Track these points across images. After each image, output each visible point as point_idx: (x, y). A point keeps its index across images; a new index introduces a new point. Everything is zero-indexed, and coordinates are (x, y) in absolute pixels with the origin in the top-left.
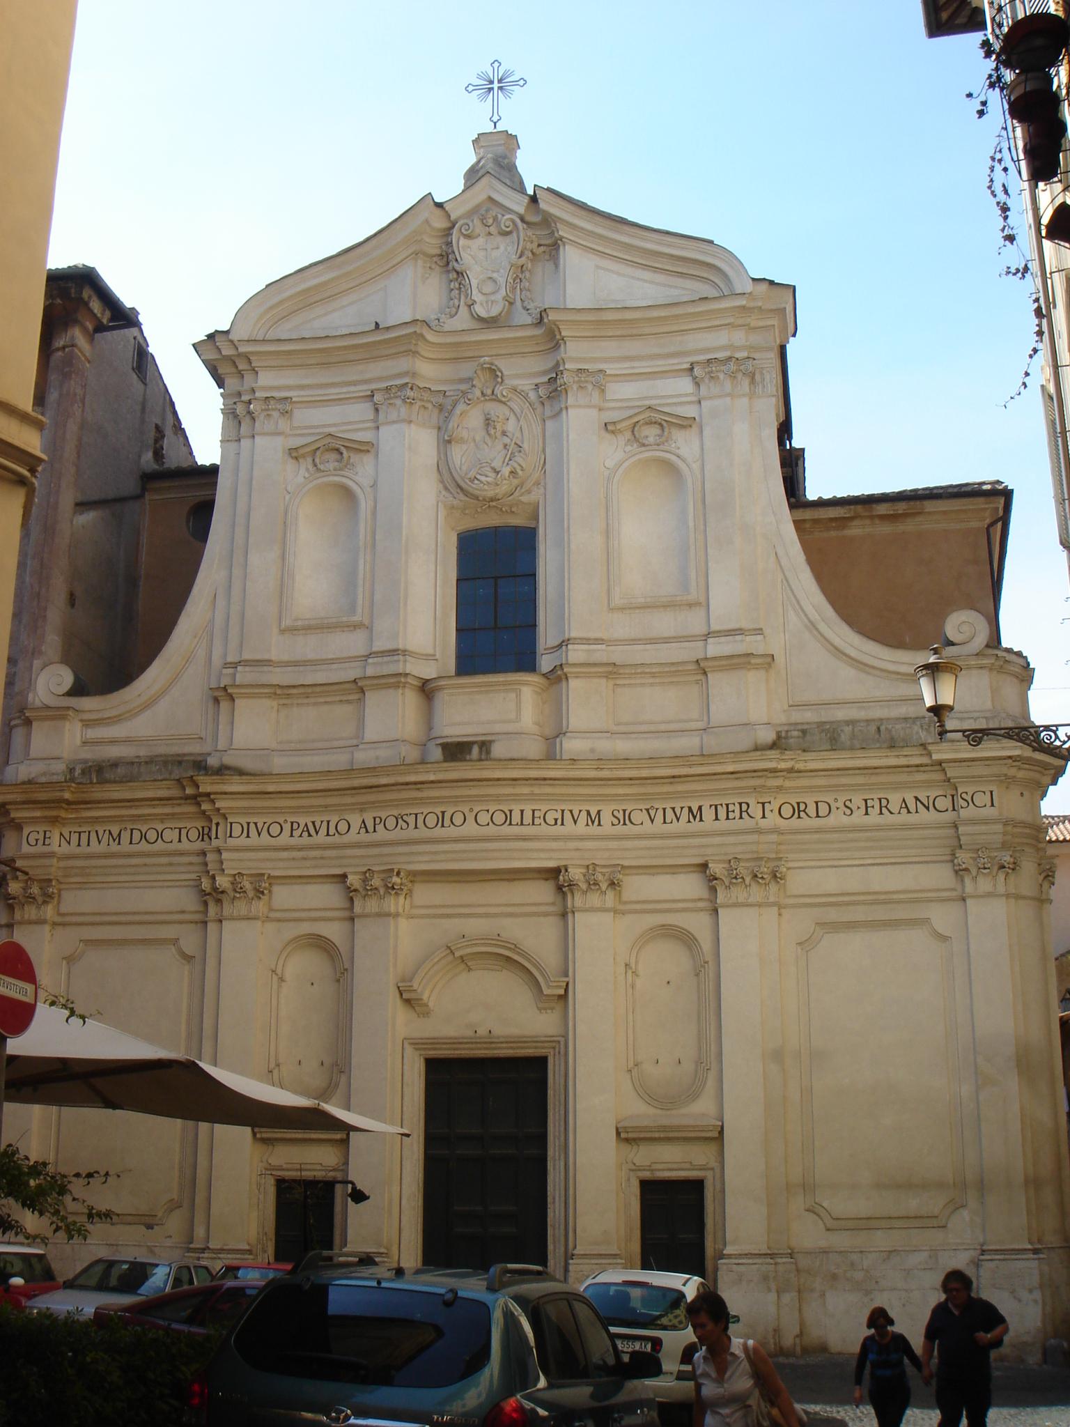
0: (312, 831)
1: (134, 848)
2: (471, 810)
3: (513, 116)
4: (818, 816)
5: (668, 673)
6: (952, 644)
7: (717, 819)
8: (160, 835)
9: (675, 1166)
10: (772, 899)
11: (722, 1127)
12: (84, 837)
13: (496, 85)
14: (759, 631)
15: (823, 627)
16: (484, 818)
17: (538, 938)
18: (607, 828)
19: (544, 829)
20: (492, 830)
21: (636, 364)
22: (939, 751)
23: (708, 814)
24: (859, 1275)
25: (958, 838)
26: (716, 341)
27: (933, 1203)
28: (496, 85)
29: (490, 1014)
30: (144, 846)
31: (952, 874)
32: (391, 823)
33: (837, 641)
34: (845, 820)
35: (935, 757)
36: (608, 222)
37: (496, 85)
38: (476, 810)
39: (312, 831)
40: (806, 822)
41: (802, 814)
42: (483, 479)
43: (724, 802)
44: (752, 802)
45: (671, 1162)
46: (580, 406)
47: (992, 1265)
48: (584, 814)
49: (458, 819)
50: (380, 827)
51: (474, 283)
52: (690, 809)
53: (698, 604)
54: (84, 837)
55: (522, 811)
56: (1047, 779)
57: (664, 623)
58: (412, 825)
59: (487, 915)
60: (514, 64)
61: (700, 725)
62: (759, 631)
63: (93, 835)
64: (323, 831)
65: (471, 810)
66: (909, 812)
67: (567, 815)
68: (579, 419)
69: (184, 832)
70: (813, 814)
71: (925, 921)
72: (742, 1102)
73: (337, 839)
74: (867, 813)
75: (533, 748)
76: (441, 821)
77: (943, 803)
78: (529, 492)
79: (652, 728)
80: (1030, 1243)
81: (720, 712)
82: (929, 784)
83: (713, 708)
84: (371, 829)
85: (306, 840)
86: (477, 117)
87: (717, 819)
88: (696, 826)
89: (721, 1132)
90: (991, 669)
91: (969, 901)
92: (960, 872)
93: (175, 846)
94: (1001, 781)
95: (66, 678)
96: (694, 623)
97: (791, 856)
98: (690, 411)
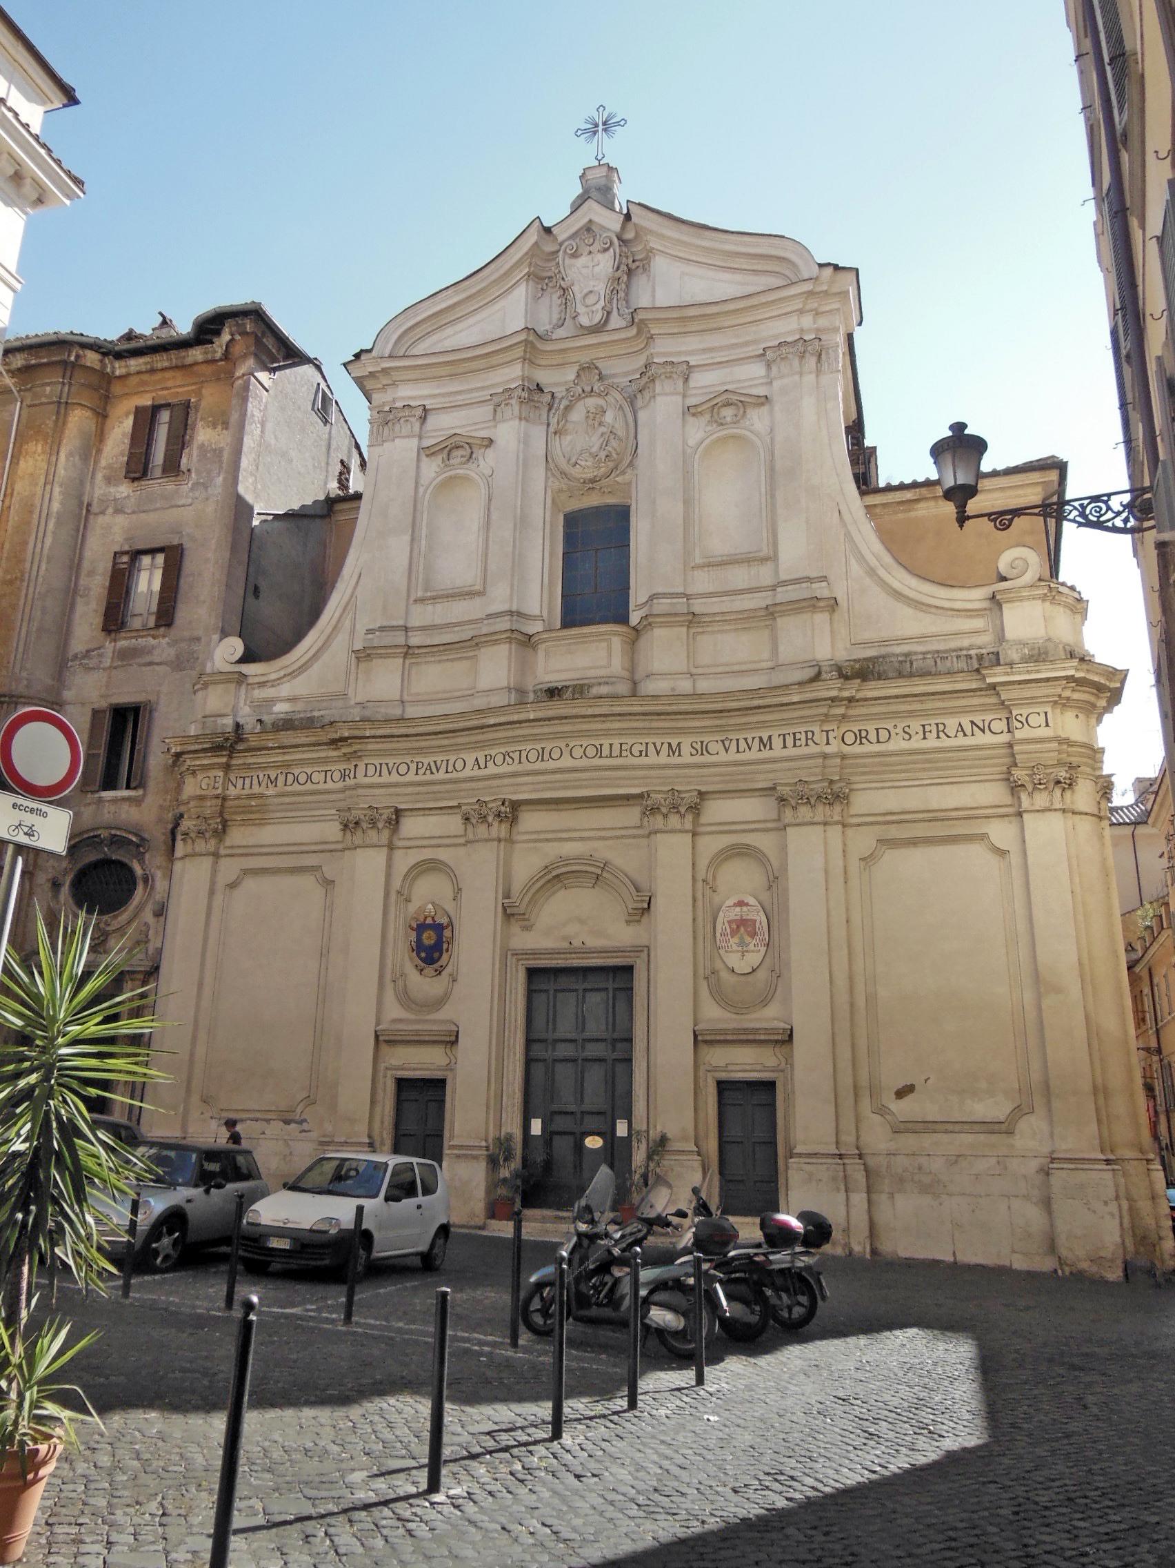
0: (434, 770)
1: (289, 789)
2: (567, 745)
3: (613, 149)
4: (878, 742)
5: (745, 620)
6: (1004, 579)
7: (785, 747)
8: (309, 778)
9: (748, 1067)
10: (836, 818)
11: (791, 1030)
12: (248, 781)
13: (602, 126)
14: (824, 579)
15: (882, 572)
16: (578, 752)
17: (625, 858)
18: (686, 758)
19: (631, 761)
20: (584, 762)
21: (714, 354)
22: (995, 675)
23: (778, 743)
24: (927, 1180)
25: (1013, 755)
26: (785, 328)
27: (993, 1108)
28: (601, 127)
29: (578, 925)
30: (296, 787)
31: (1008, 791)
32: (499, 759)
33: (896, 585)
34: (904, 745)
35: (989, 680)
36: (692, 230)
37: (602, 126)
38: (571, 745)
39: (434, 770)
40: (868, 748)
41: (864, 741)
42: (583, 463)
43: (791, 731)
44: (817, 729)
45: (745, 1063)
46: (666, 394)
47: (1063, 1174)
48: (666, 746)
49: (555, 755)
50: (490, 764)
51: (579, 296)
52: (761, 739)
53: (767, 559)
54: (248, 781)
55: (611, 745)
56: (1102, 703)
57: (739, 577)
58: (517, 761)
59: (582, 839)
60: (616, 108)
61: (770, 664)
62: (824, 579)
63: (255, 778)
64: (443, 769)
65: (567, 745)
66: (965, 735)
67: (651, 747)
68: (663, 408)
69: (329, 774)
70: (874, 739)
71: (983, 837)
72: (807, 1007)
73: (455, 775)
74: (925, 738)
75: (623, 688)
76: (541, 756)
77: (999, 726)
78: (623, 473)
79: (727, 669)
80: (1102, 1151)
81: (787, 651)
82: (984, 709)
83: (781, 648)
84: (482, 766)
85: (429, 777)
86: (585, 155)
87: (785, 747)
88: (766, 754)
89: (791, 1036)
90: (1044, 601)
91: (1025, 816)
92: (1015, 788)
93: (321, 786)
94: (1055, 702)
95: (236, 646)
96: (765, 575)
97: (857, 778)
98: (761, 391)
